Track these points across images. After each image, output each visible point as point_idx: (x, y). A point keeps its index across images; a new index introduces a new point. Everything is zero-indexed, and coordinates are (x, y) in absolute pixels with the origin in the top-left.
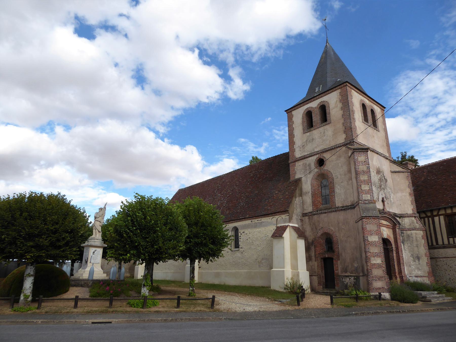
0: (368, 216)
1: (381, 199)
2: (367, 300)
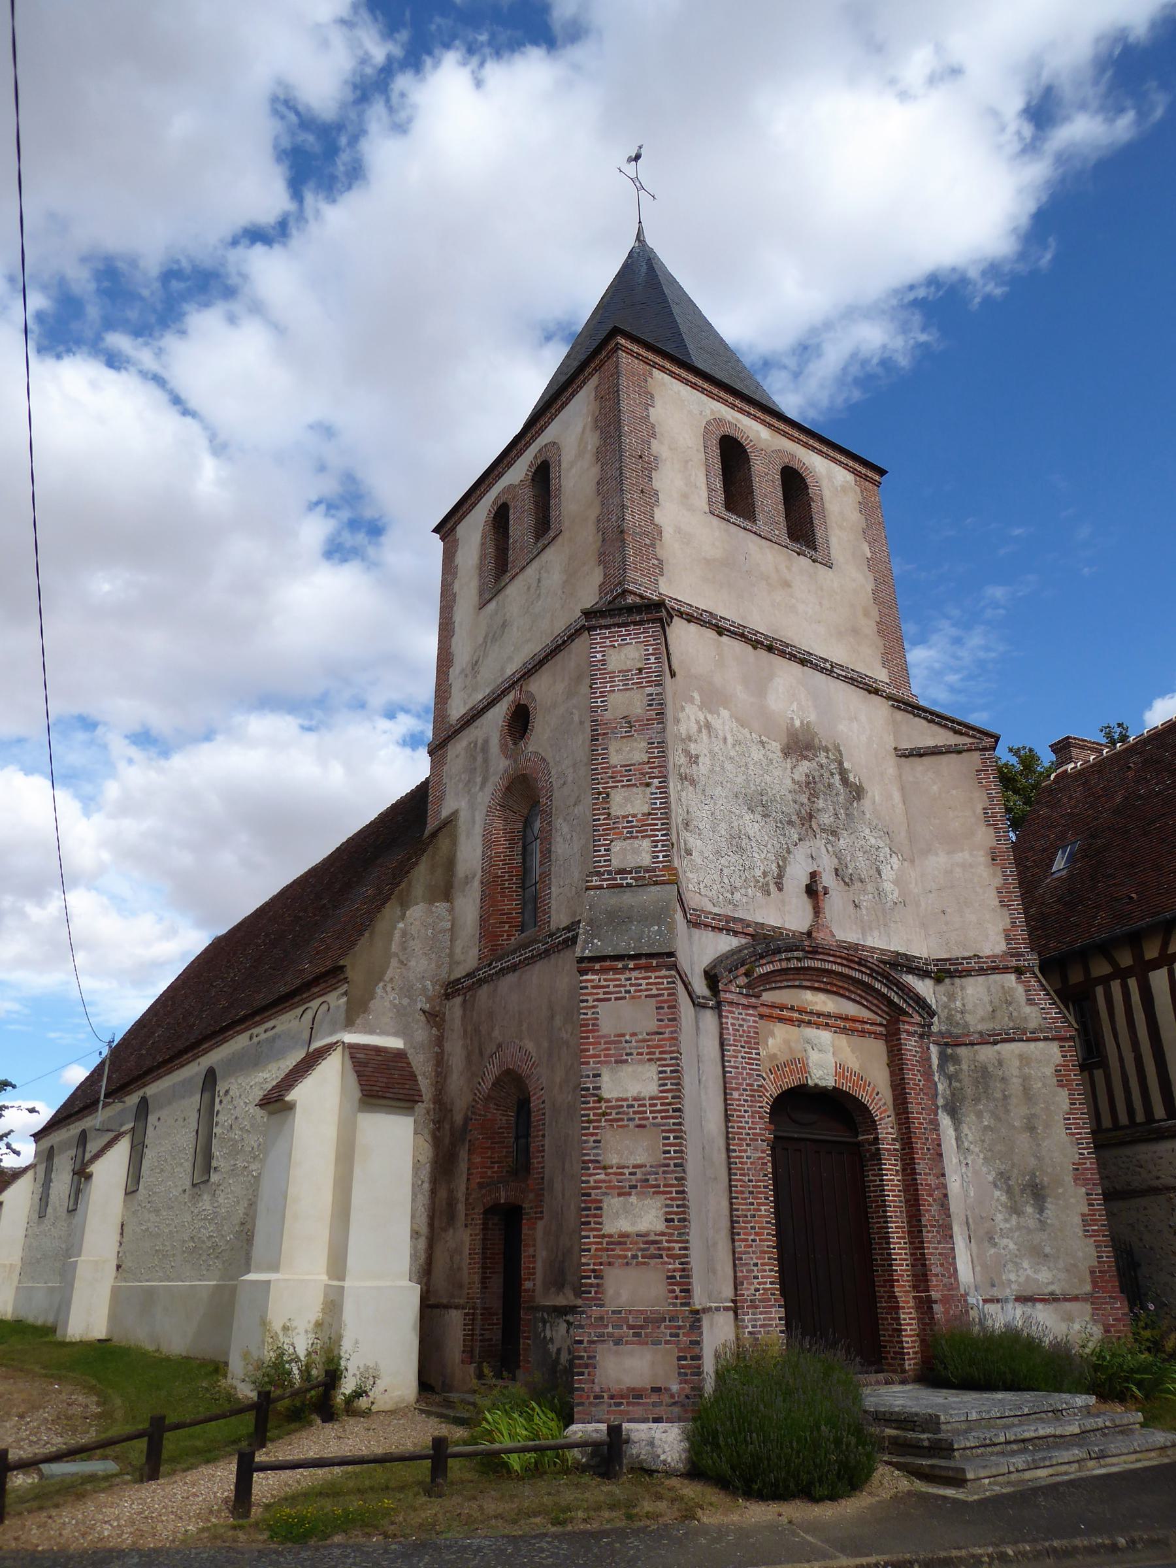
0: (609, 951)
1: (806, 880)
2: (535, 1471)
